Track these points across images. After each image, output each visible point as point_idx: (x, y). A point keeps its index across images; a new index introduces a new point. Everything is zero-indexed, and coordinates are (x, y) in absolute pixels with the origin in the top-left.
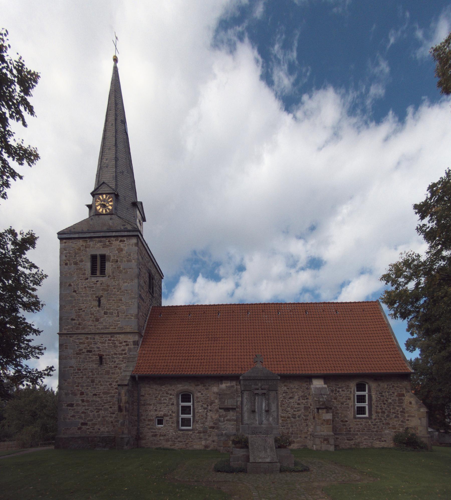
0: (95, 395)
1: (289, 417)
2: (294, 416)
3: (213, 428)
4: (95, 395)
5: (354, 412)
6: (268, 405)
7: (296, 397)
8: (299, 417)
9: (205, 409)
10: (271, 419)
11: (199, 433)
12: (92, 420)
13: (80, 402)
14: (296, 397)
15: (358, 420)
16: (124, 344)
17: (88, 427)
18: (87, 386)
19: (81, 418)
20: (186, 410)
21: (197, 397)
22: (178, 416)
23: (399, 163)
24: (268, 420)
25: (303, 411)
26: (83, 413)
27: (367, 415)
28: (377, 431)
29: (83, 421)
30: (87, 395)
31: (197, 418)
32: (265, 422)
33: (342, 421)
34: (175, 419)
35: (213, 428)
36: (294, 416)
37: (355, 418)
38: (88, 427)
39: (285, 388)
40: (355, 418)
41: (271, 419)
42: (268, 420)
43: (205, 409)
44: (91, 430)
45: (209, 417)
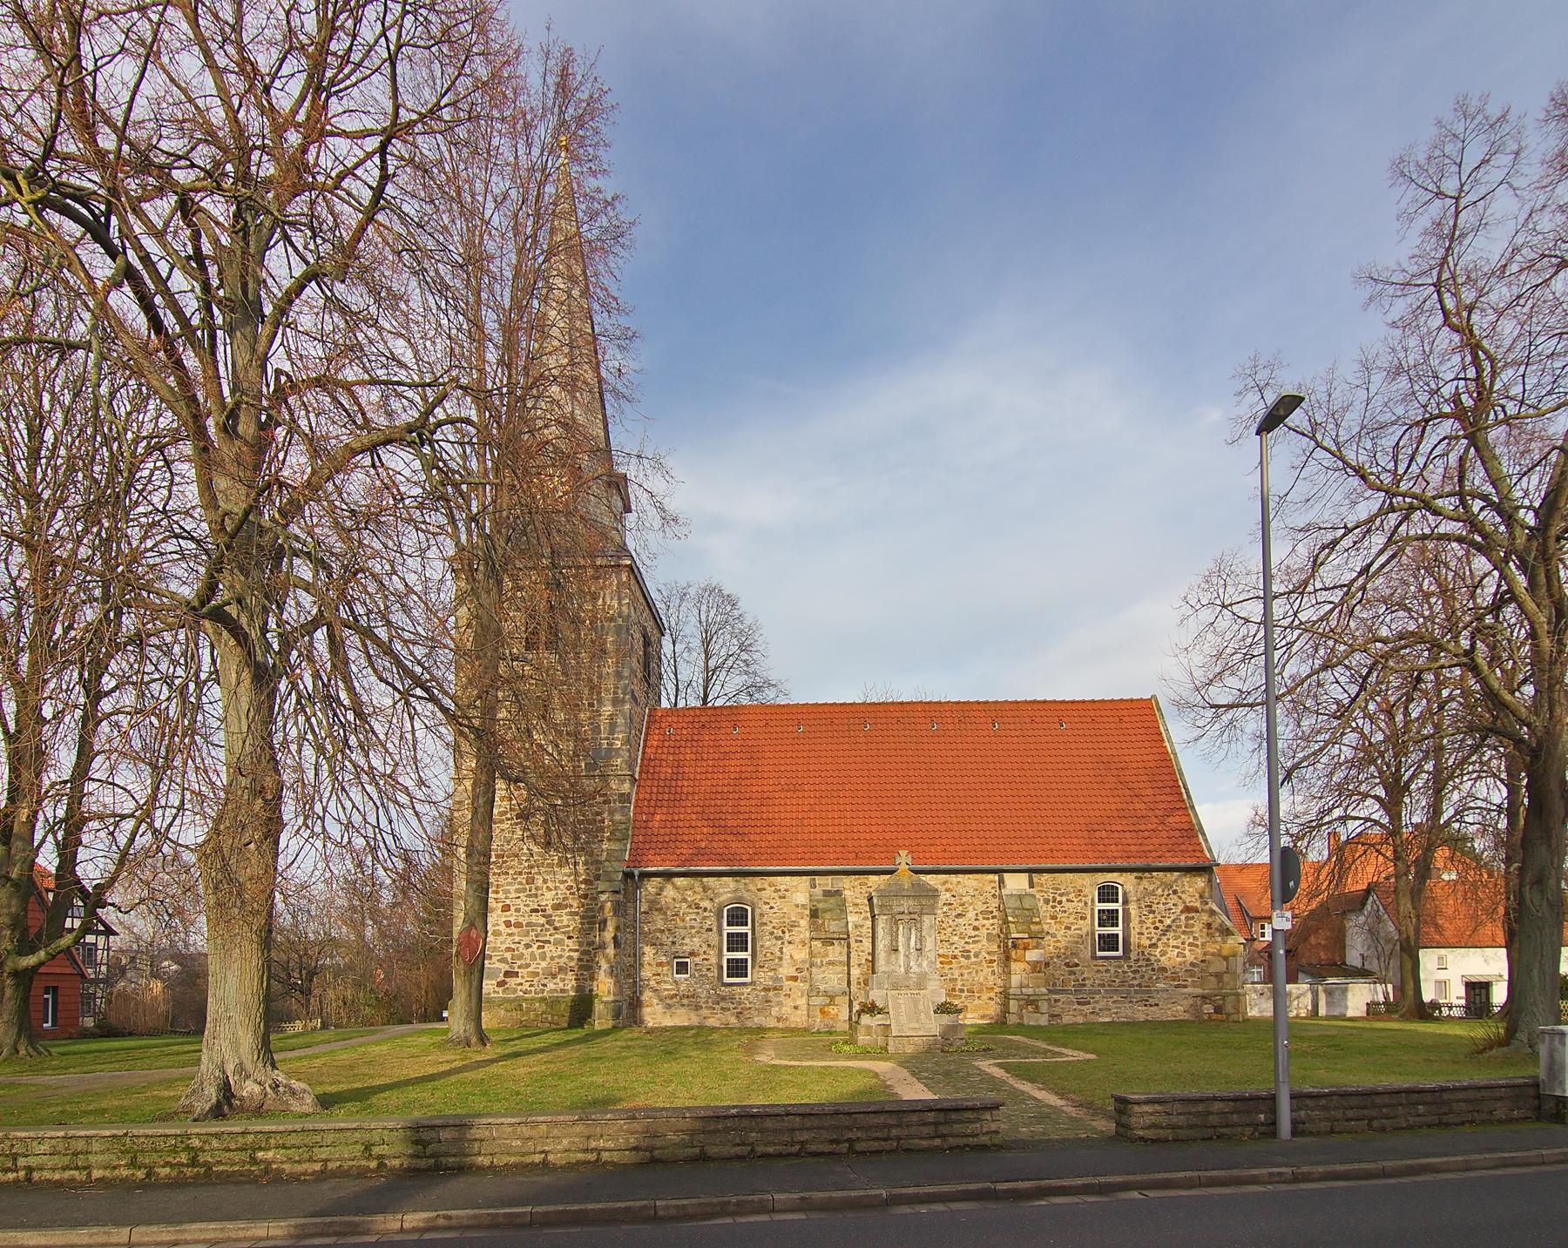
0: (536, 911)
1: (955, 957)
2: (966, 954)
3: (795, 979)
4: (536, 911)
5: (1093, 946)
6: (921, 939)
7: (971, 915)
8: (976, 956)
9: (777, 938)
10: (925, 963)
11: (766, 989)
12: (528, 966)
13: (502, 927)
14: (971, 915)
15: (1100, 962)
16: (599, 799)
17: (519, 980)
18: (517, 891)
19: (503, 960)
20: (737, 942)
21: (762, 915)
22: (720, 954)
23: (106, 1031)
24: (920, 965)
25: (985, 942)
26: (508, 949)
27: (1120, 953)
28: (1140, 985)
29: (507, 968)
30: (518, 910)
31: (760, 957)
32: (915, 969)
33: (1067, 965)
34: (714, 960)
35: (795, 979)
36: (966, 954)
37: (1094, 957)
38: (519, 980)
39: (948, 895)
40: (1094, 957)
41: (925, 963)
42: (920, 965)
43: (777, 938)
44: (526, 986)
45: (786, 957)
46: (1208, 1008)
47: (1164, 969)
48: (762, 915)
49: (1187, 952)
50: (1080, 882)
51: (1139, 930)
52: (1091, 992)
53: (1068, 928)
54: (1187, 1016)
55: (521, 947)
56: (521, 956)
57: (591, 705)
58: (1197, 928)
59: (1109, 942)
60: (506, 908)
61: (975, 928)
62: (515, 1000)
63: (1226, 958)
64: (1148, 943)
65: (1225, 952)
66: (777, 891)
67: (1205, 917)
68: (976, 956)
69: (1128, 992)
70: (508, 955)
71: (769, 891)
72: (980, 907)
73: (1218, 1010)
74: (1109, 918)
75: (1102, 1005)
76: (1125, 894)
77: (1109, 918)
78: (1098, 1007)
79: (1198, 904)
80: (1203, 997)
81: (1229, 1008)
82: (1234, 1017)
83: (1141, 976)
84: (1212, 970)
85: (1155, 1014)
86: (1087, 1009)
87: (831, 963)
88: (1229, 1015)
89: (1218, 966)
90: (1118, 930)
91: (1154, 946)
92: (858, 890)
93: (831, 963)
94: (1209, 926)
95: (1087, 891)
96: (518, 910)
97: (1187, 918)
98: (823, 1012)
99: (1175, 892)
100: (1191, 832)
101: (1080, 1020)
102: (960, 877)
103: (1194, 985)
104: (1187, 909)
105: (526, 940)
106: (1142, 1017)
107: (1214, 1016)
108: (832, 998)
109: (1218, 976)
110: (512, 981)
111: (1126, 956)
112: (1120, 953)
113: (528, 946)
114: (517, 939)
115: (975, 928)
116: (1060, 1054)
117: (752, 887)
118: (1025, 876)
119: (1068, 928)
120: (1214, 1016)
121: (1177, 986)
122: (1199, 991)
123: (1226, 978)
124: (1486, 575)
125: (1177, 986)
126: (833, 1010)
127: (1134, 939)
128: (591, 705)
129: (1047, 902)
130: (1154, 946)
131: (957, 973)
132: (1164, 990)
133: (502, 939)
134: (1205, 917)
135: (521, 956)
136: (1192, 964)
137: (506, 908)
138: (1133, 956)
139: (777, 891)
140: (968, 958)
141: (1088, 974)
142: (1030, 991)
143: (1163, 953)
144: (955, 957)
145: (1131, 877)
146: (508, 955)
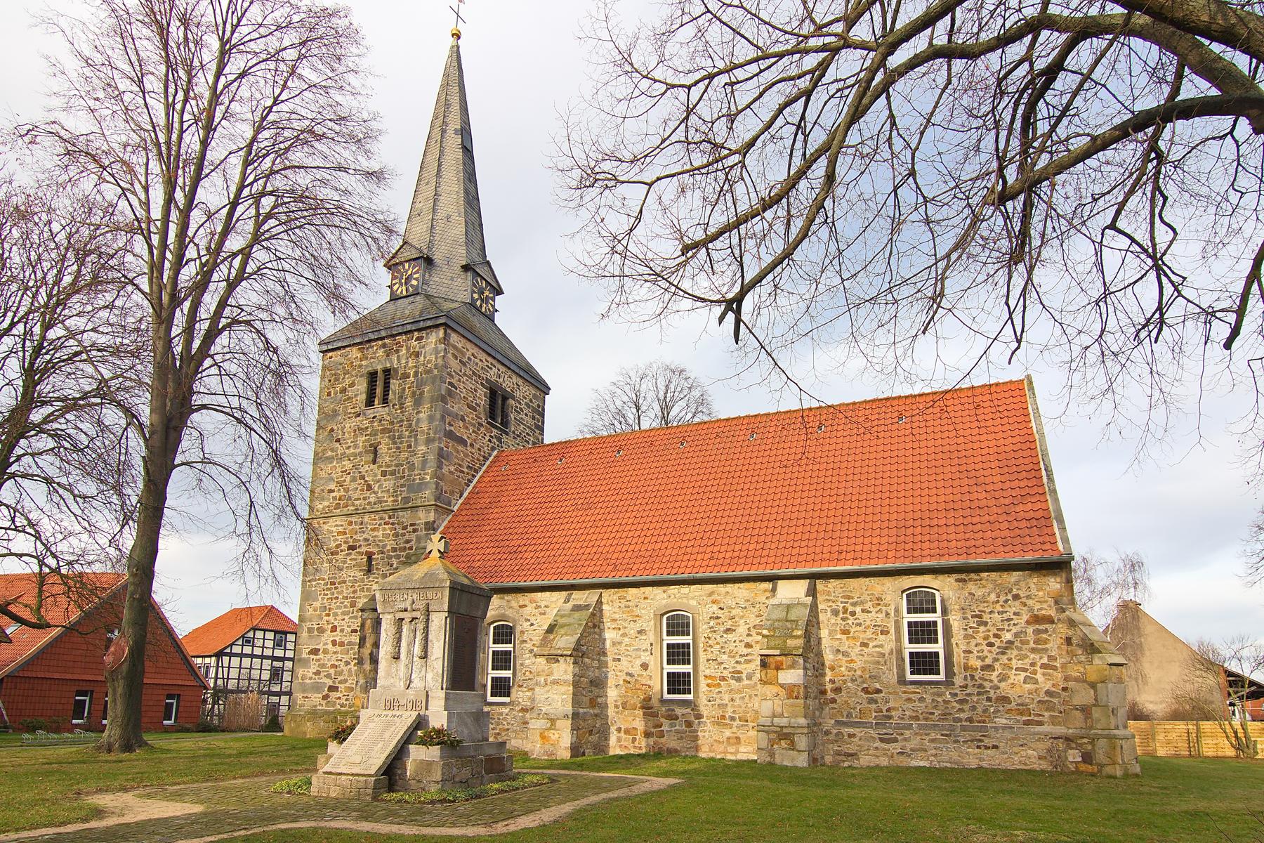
1: (723, 679)
7: (742, 629)
11: (524, 710)
12: (346, 681)
13: (330, 646)
14: (742, 629)
15: (911, 688)
17: (339, 695)
18: (344, 613)
19: (328, 676)
27: (942, 677)
28: (970, 720)
33: (866, 691)
37: (902, 681)
38: (339, 695)
39: (715, 607)
40: (902, 681)
44: (343, 701)
46: (1074, 756)
47: (1005, 699)
48: (522, 632)
49: (1039, 677)
50: (879, 588)
51: (961, 642)
52: (898, 726)
53: (865, 645)
54: (1044, 765)
55: (342, 663)
56: (341, 673)
57: (409, 446)
58: (1054, 644)
59: (924, 663)
60: (334, 629)
61: (748, 646)
62: (334, 712)
63: (1093, 685)
64: (979, 664)
65: (1092, 677)
66: (538, 607)
67: (1063, 630)
68: (749, 677)
69: (952, 728)
70: (332, 671)
71: (530, 609)
72: (754, 621)
73: (1087, 758)
74: (921, 632)
75: (914, 743)
76: (943, 601)
77: (921, 632)
78: (909, 746)
79: (1053, 613)
80: (1068, 739)
81: (1100, 756)
82: (1108, 770)
83: (975, 709)
84: (1078, 700)
85: (991, 759)
86: (894, 748)
87: (555, 682)
88: (1101, 766)
89: (1084, 696)
90: (938, 647)
91: (989, 668)
92: (617, 604)
93: (555, 682)
94: (1068, 641)
95: (888, 598)
96: (342, 631)
97: (1037, 632)
98: (543, 737)
99: (1016, 597)
100: (1046, 518)
101: (884, 762)
102: (729, 587)
103: (1053, 720)
104: (1036, 619)
105: (346, 658)
106: (974, 764)
107: (1083, 767)
108: (553, 721)
109: (1085, 710)
110: (334, 695)
111: (949, 683)
112: (942, 677)
113: (347, 663)
114: (340, 656)
115: (748, 646)
116: (630, 784)
117: (514, 604)
118: (803, 585)
119: (865, 645)
120: (1083, 767)
121: (1027, 723)
122: (1060, 730)
123: (1096, 713)
124: (192, 260)
125: (1027, 723)
126: (553, 735)
127: (958, 657)
128: (409, 446)
129: (835, 613)
130: (989, 668)
131: (727, 698)
132: (1005, 728)
133: (328, 656)
134: (1063, 630)
135: (341, 673)
136: (1048, 693)
137: (334, 629)
138: (958, 680)
139: (538, 607)
140: (739, 680)
141: (896, 702)
142: (784, 722)
143: (1003, 678)
144: (723, 679)
145: (950, 580)
146: (332, 671)
